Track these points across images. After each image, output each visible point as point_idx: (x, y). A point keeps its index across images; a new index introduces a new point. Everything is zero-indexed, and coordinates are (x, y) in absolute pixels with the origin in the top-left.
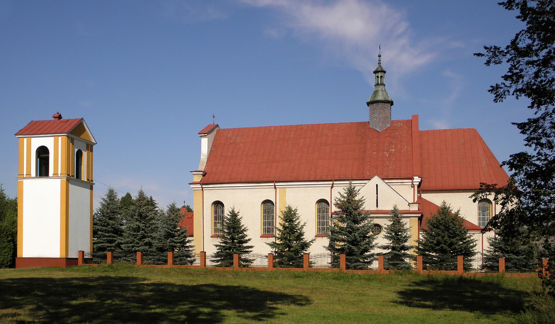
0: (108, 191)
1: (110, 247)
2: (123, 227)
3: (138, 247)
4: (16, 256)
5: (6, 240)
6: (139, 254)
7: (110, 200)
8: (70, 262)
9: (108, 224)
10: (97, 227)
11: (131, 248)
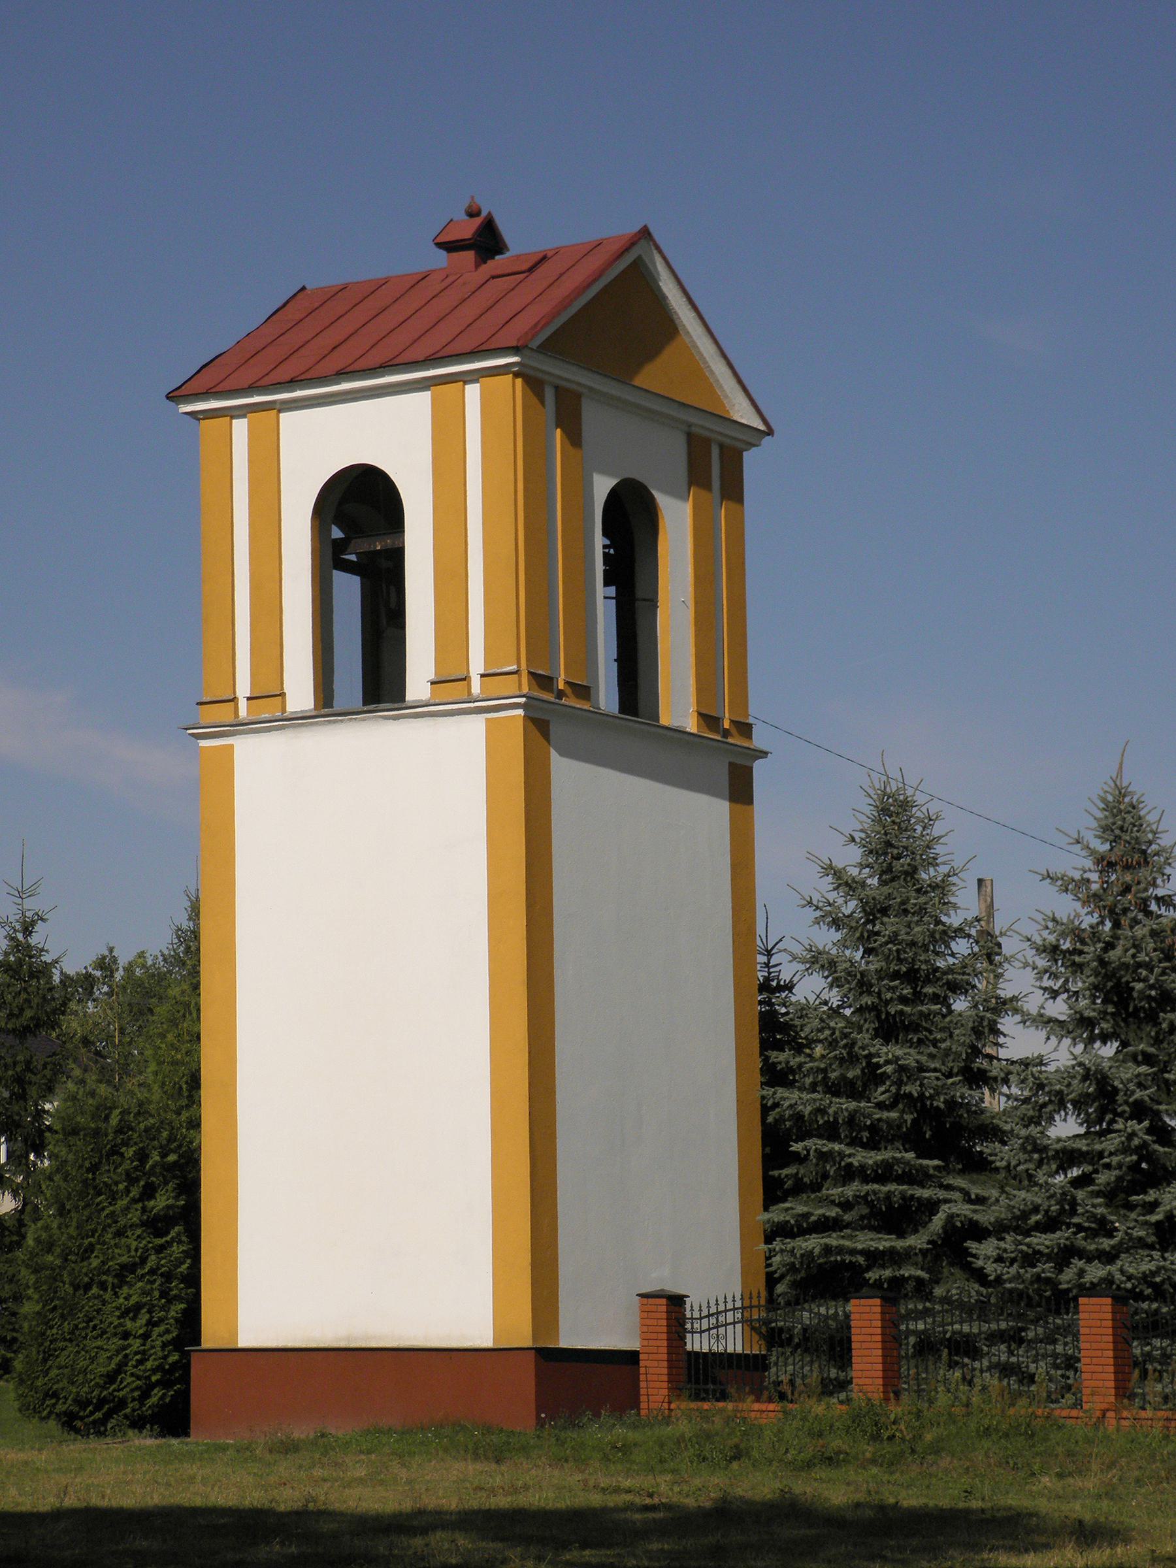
0: (867, 808)
1: (893, 1257)
2: (994, 1102)
3: (1108, 1257)
4: (196, 1338)
5: (134, 1216)
6: (1095, 1318)
7: (888, 875)
8: (568, 1382)
9: (873, 1076)
10: (789, 1097)
11: (1046, 1269)
